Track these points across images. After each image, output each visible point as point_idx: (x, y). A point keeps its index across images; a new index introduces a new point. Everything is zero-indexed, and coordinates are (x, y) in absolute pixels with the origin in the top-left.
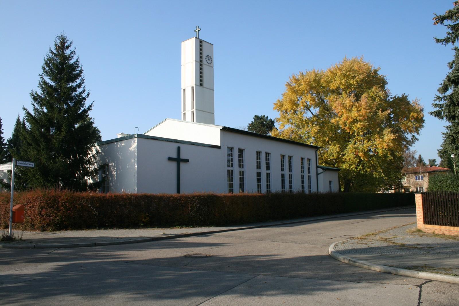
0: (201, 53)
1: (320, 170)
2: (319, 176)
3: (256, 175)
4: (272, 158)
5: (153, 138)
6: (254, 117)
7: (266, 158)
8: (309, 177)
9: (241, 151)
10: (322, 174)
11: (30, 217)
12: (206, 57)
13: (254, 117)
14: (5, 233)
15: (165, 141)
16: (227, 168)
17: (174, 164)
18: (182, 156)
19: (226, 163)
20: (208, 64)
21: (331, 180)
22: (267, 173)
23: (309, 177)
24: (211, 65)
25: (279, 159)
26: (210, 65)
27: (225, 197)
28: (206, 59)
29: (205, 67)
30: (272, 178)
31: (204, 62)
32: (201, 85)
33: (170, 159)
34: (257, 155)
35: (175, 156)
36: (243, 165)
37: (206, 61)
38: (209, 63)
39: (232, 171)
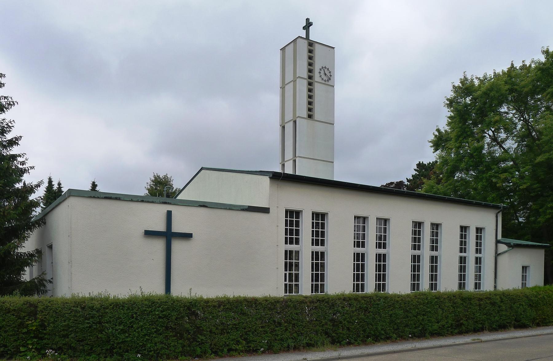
0: (310, 64)
1: (503, 248)
2: (500, 259)
3: (457, 260)
4: (392, 227)
5: (107, 196)
6: (416, 168)
7: (477, 236)
8: (478, 261)
9: (436, 227)
10: (506, 255)
11: (407, 316)
12: (320, 70)
13: (416, 168)
14: (549, 322)
15: (138, 201)
16: (284, 247)
17: (159, 245)
18: (176, 228)
19: (410, 243)
20: (323, 82)
21: (525, 264)
22: (477, 258)
23: (478, 261)
24: (330, 83)
25: (409, 228)
26: (327, 83)
27: (408, 296)
28: (320, 73)
29: (319, 89)
30: (330, 262)
31: (317, 77)
32: (310, 116)
33: (149, 234)
34: (461, 231)
35: (161, 227)
36: (437, 247)
37: (321, 76)
38: (325, 81)
39: (480, 258)
